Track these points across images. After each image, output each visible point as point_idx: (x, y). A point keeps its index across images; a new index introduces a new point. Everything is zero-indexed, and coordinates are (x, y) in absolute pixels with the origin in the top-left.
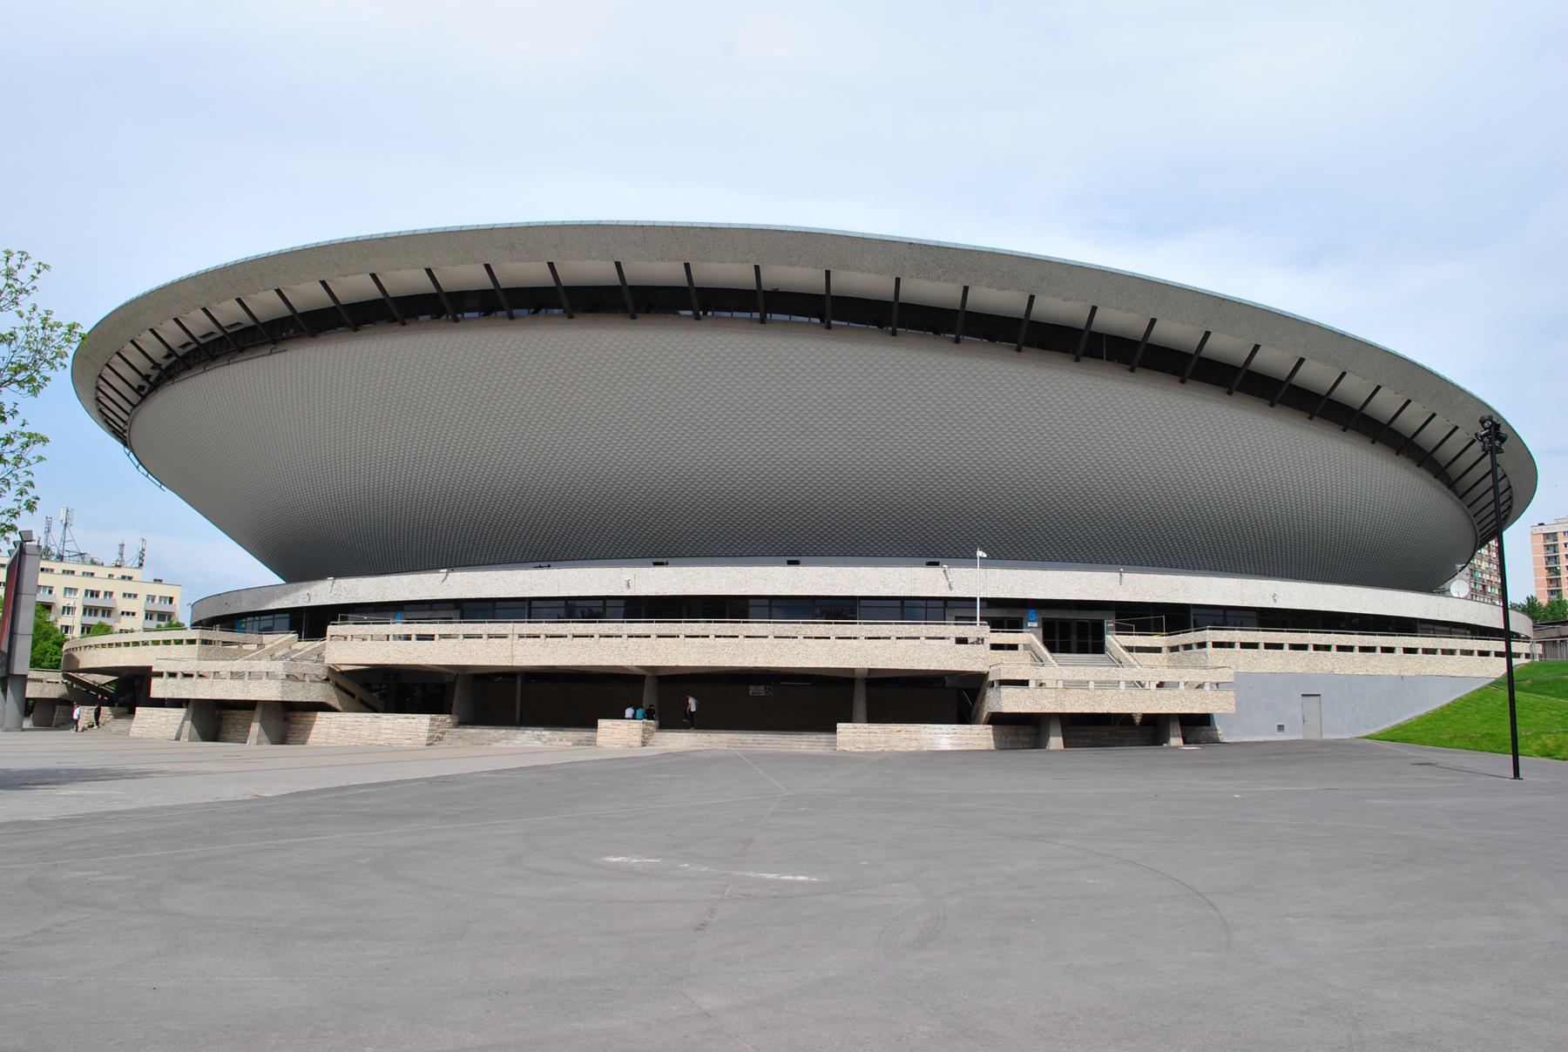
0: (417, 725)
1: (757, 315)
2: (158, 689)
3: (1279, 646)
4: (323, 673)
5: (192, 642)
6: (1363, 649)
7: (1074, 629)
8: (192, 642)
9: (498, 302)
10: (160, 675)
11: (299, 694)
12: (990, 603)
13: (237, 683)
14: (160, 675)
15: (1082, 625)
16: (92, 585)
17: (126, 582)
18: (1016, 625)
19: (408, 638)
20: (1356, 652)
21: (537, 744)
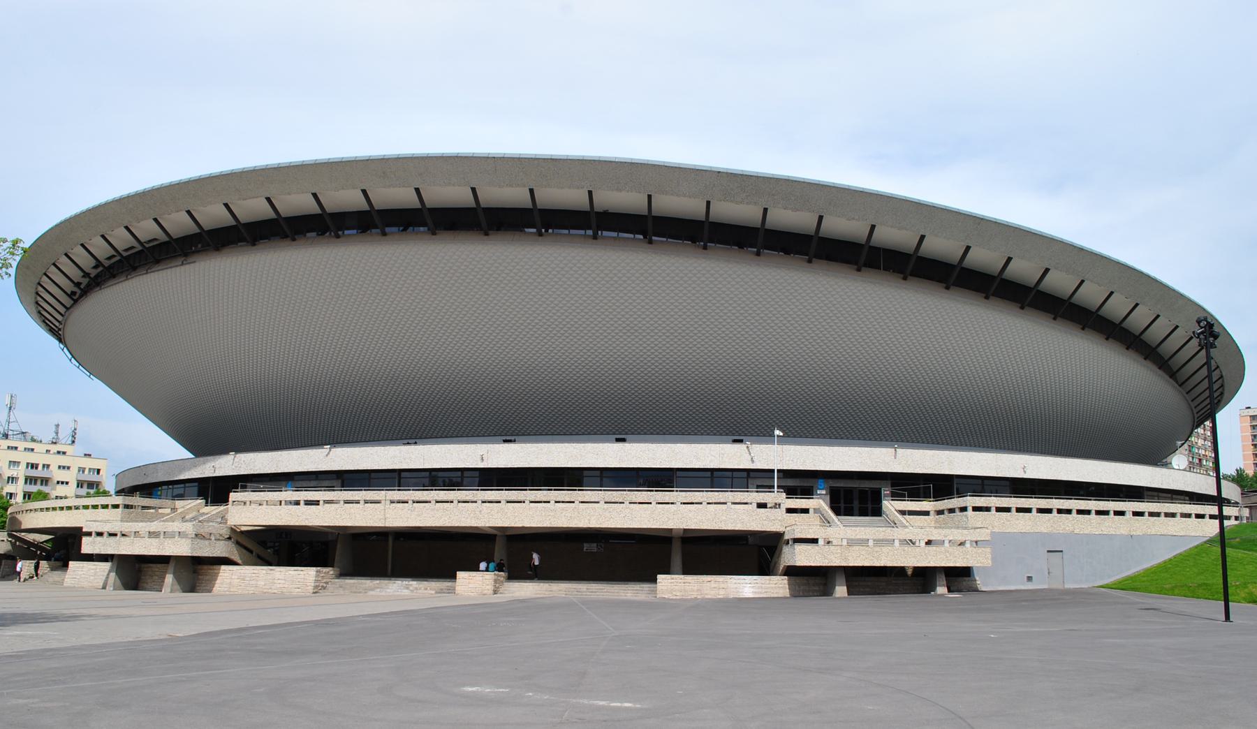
0: (306, 576)
1: (590, 232)
2: (88, 546)
3: (1069, 512)
4: (226, 533)
5: (116, 506)
6: (1099, 513)
7: (856, 496)
8: (116, 506)
9: (323, 225)
10: (89, 534)
11: (206, 550)
12: (785, 474)
13: (154, 541)
14: (89, 534)
15: (863, 492)
16: (32, 458)
17: (61, 457)
18: (807, 492)
19: (297, 503)
20: (1093, 515)
21: (406, 592)
